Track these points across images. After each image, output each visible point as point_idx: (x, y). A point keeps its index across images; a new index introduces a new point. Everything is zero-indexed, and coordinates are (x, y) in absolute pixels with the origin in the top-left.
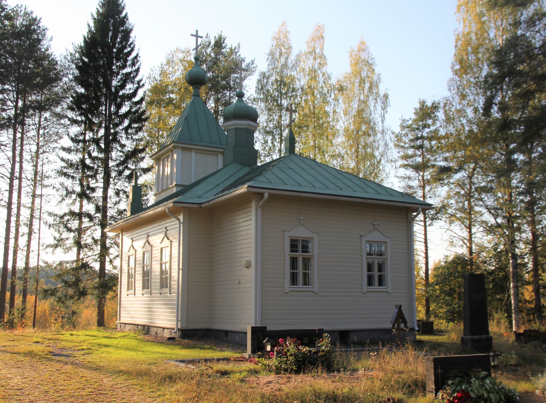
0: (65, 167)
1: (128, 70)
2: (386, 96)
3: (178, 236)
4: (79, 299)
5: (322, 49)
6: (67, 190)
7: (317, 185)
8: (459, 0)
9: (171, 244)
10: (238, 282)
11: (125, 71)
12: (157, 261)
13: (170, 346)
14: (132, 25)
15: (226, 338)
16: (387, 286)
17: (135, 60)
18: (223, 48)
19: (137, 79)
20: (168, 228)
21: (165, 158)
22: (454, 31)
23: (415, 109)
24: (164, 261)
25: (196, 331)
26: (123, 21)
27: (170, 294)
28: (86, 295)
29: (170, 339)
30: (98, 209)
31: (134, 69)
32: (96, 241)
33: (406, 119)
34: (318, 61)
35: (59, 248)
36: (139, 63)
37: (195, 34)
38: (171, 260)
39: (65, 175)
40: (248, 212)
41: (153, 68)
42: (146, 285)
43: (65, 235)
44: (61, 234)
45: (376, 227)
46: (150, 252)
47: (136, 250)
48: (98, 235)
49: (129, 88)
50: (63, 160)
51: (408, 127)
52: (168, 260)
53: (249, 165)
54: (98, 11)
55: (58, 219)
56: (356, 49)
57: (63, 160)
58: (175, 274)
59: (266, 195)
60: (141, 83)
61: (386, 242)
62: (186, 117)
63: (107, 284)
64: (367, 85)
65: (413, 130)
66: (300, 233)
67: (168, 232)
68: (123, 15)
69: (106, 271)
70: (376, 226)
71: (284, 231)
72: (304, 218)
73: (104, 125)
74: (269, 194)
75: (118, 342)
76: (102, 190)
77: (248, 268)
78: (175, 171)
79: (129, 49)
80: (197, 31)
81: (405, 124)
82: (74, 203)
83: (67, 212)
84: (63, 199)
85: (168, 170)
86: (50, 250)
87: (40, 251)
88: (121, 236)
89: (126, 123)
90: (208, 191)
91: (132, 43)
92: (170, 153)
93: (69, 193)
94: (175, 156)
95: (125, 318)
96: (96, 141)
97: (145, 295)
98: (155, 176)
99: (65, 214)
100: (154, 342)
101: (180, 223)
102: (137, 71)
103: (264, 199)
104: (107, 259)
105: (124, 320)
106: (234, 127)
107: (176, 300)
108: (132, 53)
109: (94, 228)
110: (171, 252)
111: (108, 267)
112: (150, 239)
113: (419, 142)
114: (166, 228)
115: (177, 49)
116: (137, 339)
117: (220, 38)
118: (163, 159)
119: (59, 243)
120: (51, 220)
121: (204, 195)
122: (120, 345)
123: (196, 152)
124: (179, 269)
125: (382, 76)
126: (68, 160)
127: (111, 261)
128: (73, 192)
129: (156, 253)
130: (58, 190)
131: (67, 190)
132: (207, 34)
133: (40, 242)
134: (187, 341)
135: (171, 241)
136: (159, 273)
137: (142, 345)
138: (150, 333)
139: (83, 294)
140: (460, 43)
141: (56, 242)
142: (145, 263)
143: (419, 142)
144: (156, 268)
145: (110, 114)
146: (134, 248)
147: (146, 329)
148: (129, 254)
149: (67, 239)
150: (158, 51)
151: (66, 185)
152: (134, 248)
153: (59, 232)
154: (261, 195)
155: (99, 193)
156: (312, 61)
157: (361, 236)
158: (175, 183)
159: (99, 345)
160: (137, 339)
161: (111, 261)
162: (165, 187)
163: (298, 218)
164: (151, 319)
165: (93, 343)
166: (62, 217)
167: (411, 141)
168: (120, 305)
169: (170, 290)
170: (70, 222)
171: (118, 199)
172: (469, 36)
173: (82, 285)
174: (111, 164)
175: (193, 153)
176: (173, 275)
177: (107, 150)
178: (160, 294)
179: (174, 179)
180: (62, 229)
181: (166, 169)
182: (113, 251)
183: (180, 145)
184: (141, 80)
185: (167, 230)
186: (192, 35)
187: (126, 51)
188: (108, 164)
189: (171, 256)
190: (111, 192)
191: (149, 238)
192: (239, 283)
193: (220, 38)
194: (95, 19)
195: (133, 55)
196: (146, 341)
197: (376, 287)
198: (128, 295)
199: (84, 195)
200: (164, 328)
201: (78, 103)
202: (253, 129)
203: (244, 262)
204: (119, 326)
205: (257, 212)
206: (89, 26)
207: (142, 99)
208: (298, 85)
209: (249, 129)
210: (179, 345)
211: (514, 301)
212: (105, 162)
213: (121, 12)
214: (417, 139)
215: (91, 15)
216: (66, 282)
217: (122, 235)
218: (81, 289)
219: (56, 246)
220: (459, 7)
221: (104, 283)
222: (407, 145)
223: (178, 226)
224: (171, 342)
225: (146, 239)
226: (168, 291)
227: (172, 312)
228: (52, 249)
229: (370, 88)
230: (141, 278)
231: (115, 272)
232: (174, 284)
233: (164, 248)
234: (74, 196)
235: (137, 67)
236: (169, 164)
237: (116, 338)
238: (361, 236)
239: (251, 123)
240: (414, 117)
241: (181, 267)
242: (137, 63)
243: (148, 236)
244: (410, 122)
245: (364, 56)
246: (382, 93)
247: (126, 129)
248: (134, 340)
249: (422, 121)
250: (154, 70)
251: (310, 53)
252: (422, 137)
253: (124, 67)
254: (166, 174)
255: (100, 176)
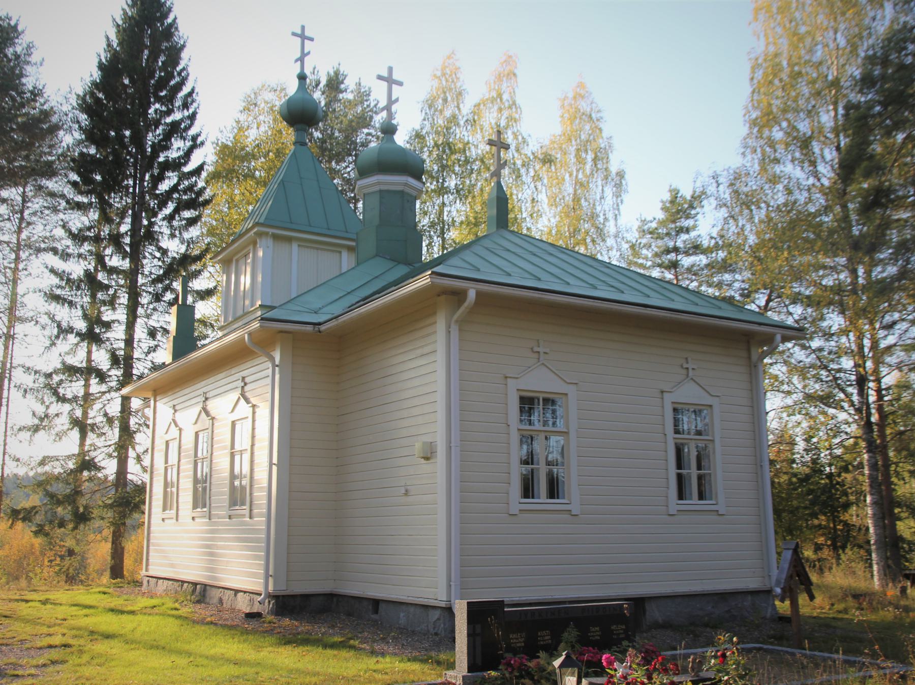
0: (59, 287)
1: (177, 116)
2: (621, 175)
3: (269, 395)
4: (75, 528)
5: (513, 93)
6: (59, 326)
7: (572, 281)
8: (756, 2)
9: (254, 413)
10: (403, 491)
11: (169, 120)
12: (224, 448)
13: (251, 637)
14: (185, 37)
15: (374, 616)
16: (716, 497)
17: (190, 100)
18: (342, 92)
19: (192, 132)
20: (247, 380)
21: (241, 257)
22: (749, 53)
23: (662, 202)
24: (237, 447)
25: (306, 597)
26: (169, 32)
27: (251, 517)
28: (89, 520)
29: (250, 616)
30: (115, 360)
31: (186, 113)
32: (110, 420)
33: (648, 219)
34: (506, 113)
35: (42, 432)
36: (195, 105)
37: (299, 32)
38: (253, 445)
39: (57, 298)
40: (428, 335)
41: (222, 128)
42: (201, 498)
43: (55, 408)
44: (48, 407)
45: (691, 373)
46: (210, 431)
47: (180, 430)
48: (114, 409)
49: (178, 146)
50: (53, 271)
51: (651, 233)
52: (247, 445)
53: (407, 263)
54: (125, 13)
55: (42, 380)
56: (571, 95)
57: (53, 271)
58: (261, 475)
59: (472, 294)
60: (200, 140)
61: (711, 406)
62: (282, 180)
63: (129, 501)
64: (590, 157)
65: (660, 237)
66: (540, 382)
67: (246, 388)
68: (170, 20)
69: (129, 477)
70: (690, 370)
71: (506, 377)
72: (547, 350)
73: (130, 212)
74: (478, 294)
75: (134, 625)
76: (124, 327)
77: (427, 459)
78: (260, 279)
79: (177, 79)
80: (303, 28)
81: (646, 227)
82: (73, 351)
83: (59, 366)
84: (53, 344)
85: (246, 281)
86: (25, 435)
87: (8, 438)
88: (152, 402)
89: (170, 207)
90: (331, 303)
91: (184, 69)
92: (251, 247)
93: (64, 331)
94: (260, 254)
95: (158, 566)
96: (115, 240)
97: (197, 520)
98: (224, 296)
99: (56, 372)
100: (216, 624)
101: (274, 366)
102: (193, 117)
103: (466, 304)
104: (132, 453)
105: (155, 570)
106: (377, 188)
107: (265, 532)
108: (184, 88)
109: (108, 396)
110: (253, 429)
111: (132, 467)
112: (212, 405)
113: (672, 256)
114: (243, 378)
115: (263, 86)
116: (178, 617)
117: (337, 73)
118: (237, 261)
119: (41, 424)
120: (28, 380)
121: (326, 309)
122: (137, 635)
123: (299, 246)
124: (271, 464)
125: (615, 142)
126: (64, 272)
127: (139, 459)
128: (70, 330)
129: (223, 433)
130: (44, 328)
131: (59, 326)
132: (314, 68)
133: (9, 421)
134: (287, 621)
135: (254, 406)
136: (227, 474)
137: (188, 632)
138: (207, 600)
139: (82, 518)
140: (759, 74)
141: (36, 421)
142: (200, 455)
143: (672, 256)
144: (222, 462)
145: (142, 194)
146: (176, 425)
147: (200, 592)
148: (168, 437)
149: (57, 415)
150: (228, 95)
151: (58, 318)
152: (176, 425)
153: (43, 402)
154: (458, 296)
155: (118, 334)
156: (495, 114)
157: (662, 392)
158: (259, 303)
159: (92, 632)
160: (178, 617)
161: (139, 459)
162: (240, 313)
163: (536, 349)
164: (211, 570)
165: (79, 629)
166: (49, 376)
167: (656, 255)
168: (148, 541)
169: (251, 510)
170: (63, 385)
171: (153, 343)
172: (777, 60)
173: (82, 502)
174: (141, 280)
175: (295, 246)
176: (257, 476)
177: (135, 256)
178: (230, 517)
179: (259, 294)
180: (49, 398)
181: (242, 277)
182: (142, 440)
183: (271, 231)
184: (198, 135)
185: (246, 384)
186: (294, 34)
187: (172, 83)
188: (137, 281)
189: (253, 437)
190: (140, 332)
191: (208, 403)
192: (407, 493)
193: (337, 73)
194: (118, 26)
195: (186, 90)
196: (195, 622)
197: (693, 502)
198: (163, 520)
199: (92, 336)
200: (237, 591)
201: (83, 165)
202: (414, 193)
203: (418, 446)
204: (145, 583)
205: (448, 327)
206: (108, 38)
207: (200, 169)
208: (473, 153)
209: (408, 194)
210: (270, 632)
211: (875, 529)
212: (132, 274)
213: (166, 16)
214: (668, 251)
215: (111, 19)
216: (52, 496)
217: (155, 401)
218: (81, 510)
219: (36, 429)
220: (757, 11)
221: (123, 498)
222: (649, 263)
223: (270, 371)
224: (252, 624)
225: (201, 405)
226: (247, 512)
227: (256, 557)
228: (29, 433)
229: (595, 160)
230: (190, 485)
231: (146, 478)
232: (260, 497)
233: (239, 425)
234: (72, 339)
235: (191, 111)
236: (249, 269)
237: (132, 612)
238: (662, 392)
239: (412, 181)
240: (661, 215)
241: (275, 460)
242: (191, 104)
243: (207, 399)
244: (654, 225)
245: (584, 106)
246: (614, 169)
247: (170, 218)
248: (171, 620)
249: (674, 222)
250: (224, 130)
251: (493, 101)
252: (676, 250)
253: (169, 112)
254: (242, 288)
255: (124, 299)
